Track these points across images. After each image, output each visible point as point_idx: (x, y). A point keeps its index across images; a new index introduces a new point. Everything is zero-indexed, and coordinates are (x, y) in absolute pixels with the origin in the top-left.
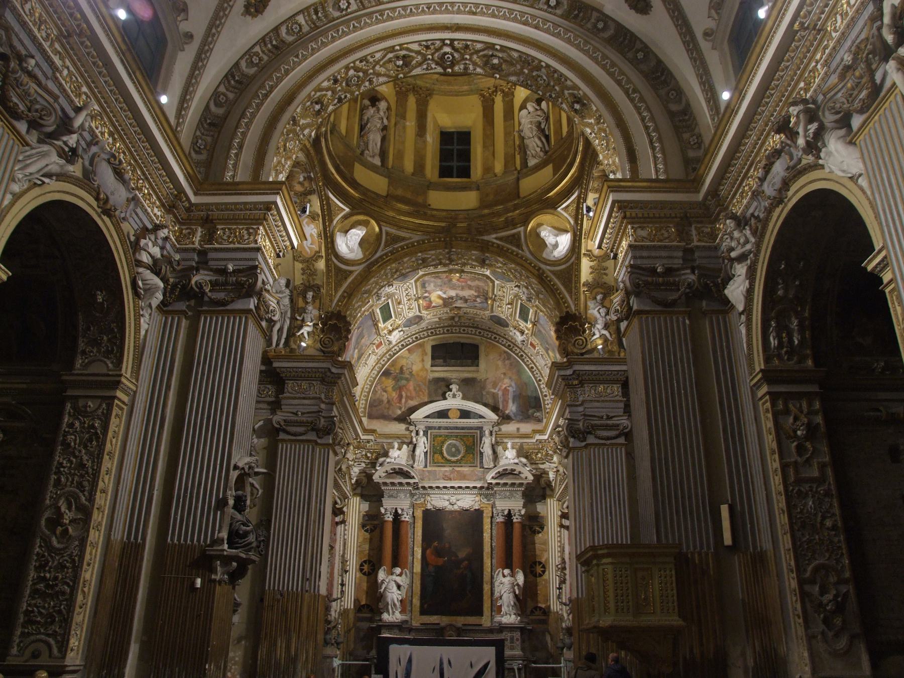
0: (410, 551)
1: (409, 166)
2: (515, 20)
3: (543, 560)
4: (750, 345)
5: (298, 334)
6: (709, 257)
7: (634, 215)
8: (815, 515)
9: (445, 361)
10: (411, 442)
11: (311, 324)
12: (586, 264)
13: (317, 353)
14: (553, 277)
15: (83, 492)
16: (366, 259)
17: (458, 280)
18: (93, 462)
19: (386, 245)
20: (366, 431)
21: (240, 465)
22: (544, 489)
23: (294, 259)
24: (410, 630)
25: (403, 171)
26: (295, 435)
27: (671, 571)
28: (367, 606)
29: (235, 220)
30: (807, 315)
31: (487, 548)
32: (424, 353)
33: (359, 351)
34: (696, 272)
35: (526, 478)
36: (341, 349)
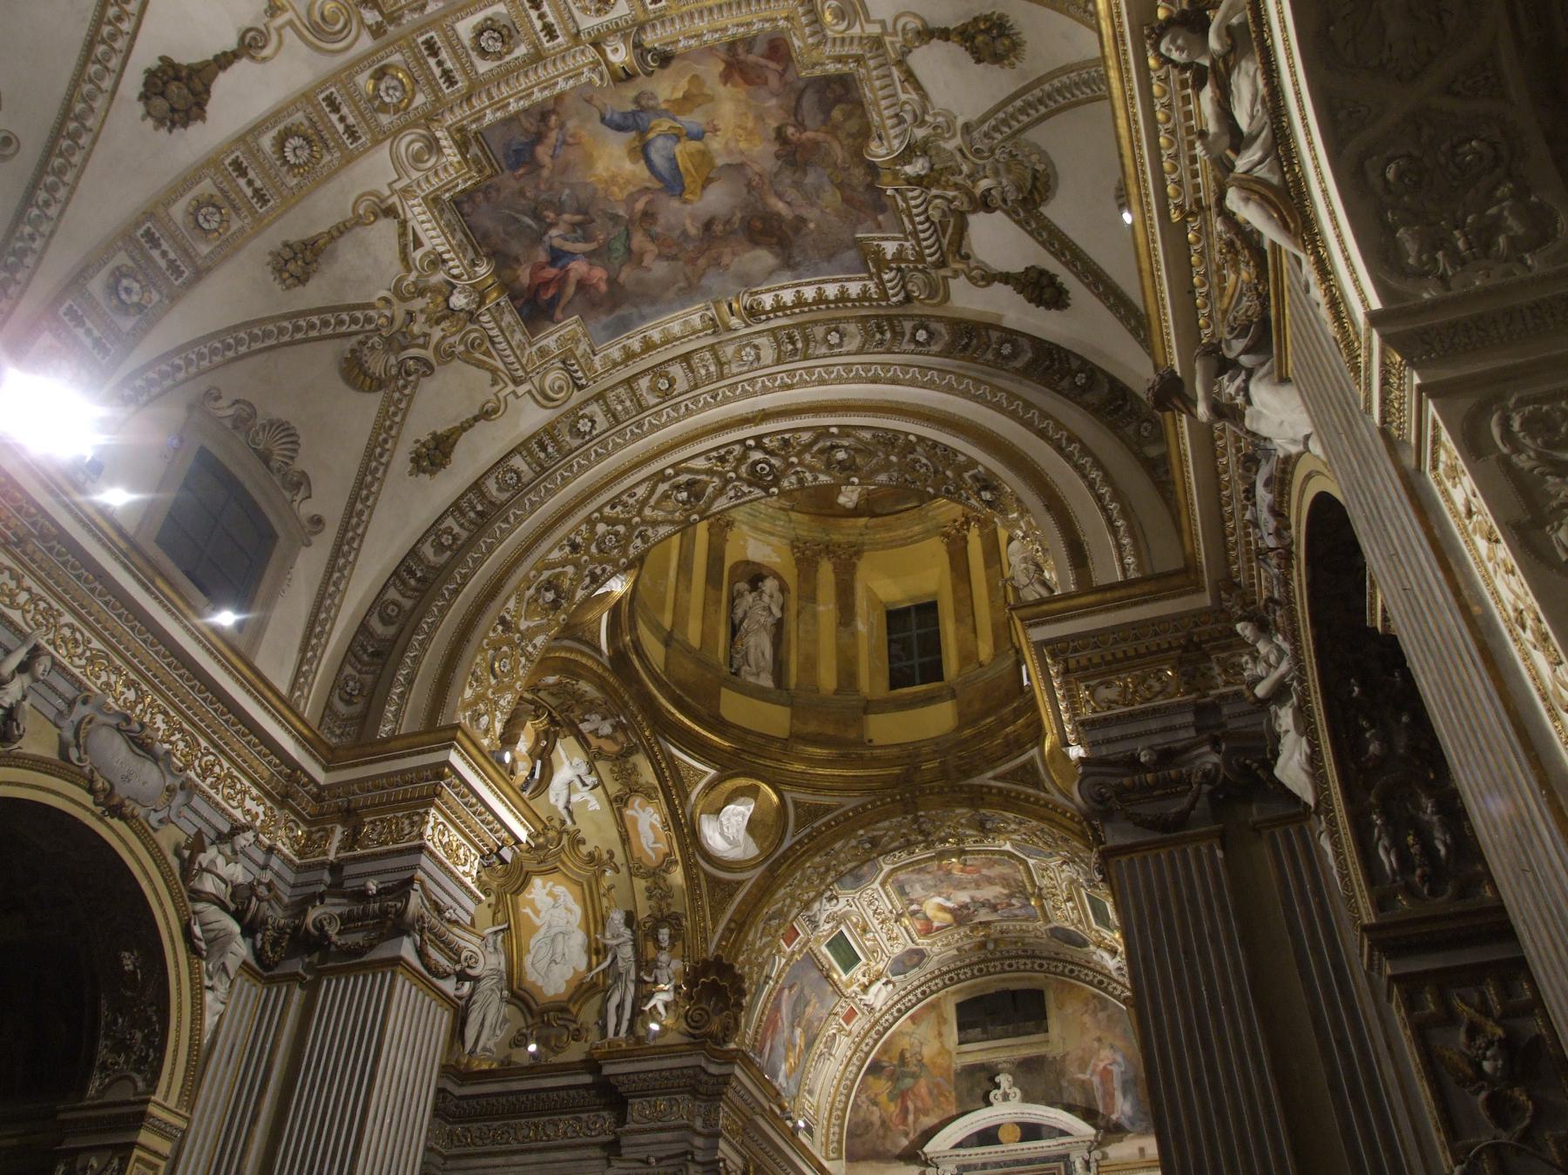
1: (827, 679)
2: (858, 379)
5: (647, 1008)
7: (1083, 662)
9: (985, 1031)
13: (687, 1040)
16: (765, 856)
19: (799, 825)
25: (818, 690)
29: (392, 805)
32: (942, 1020)
33: (805, 1031)
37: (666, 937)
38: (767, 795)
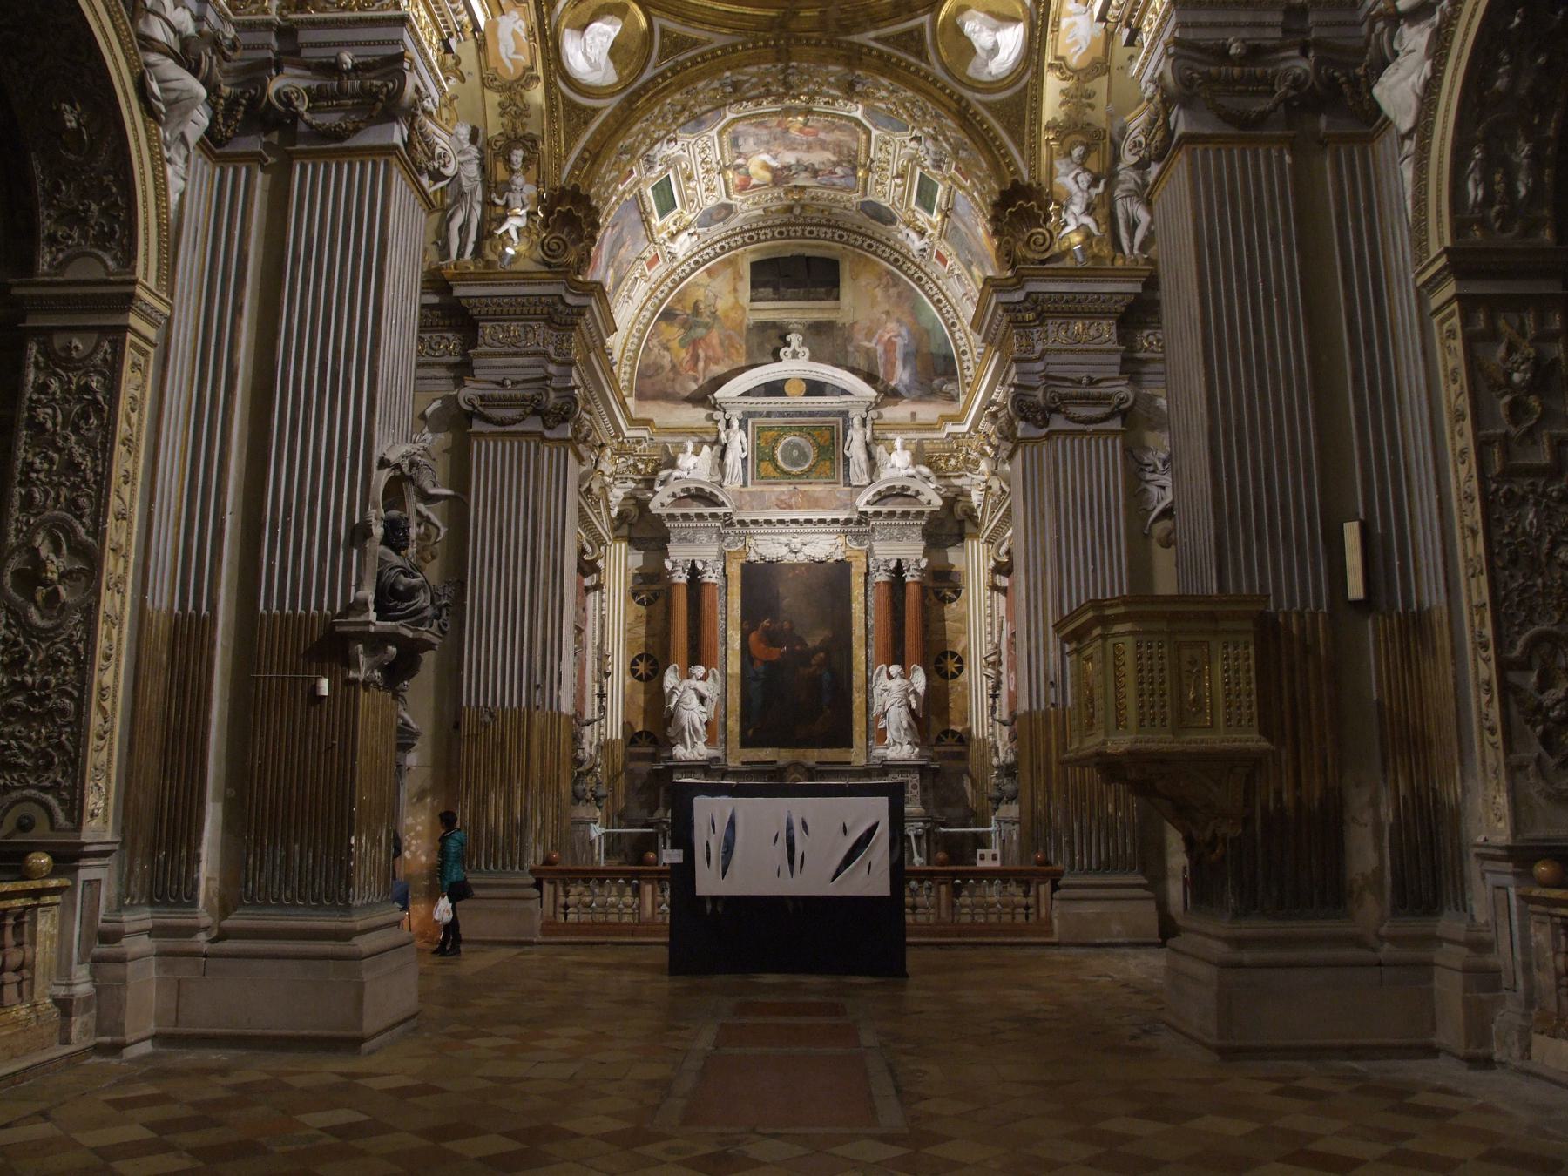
0: (720, 635)
3: (959, 650)
4: (1420, 202)
6: (1340, 24)
8: (1539, 539)
9: (776, 288)
10: (717, 441)
11: (523, 212)
12: (1053, 86)
13: (531, 267)
14: (986, 114)
15: (80, 517)
17: (801, 131)
18: (95, 458)
19: (663, 55)
20: (633, 422)
21: (393, 457)
22: (961, 522)
23: (483, 85)
24: (724, 774)
26: (501, 423)
27: (1247, 648)
28: (646, 734)
30: (1551, 133)
31: (858, 631)
32: (738, 277)
33: (616, 272)
34: (1311, 54)
35: (929, 502)
36: (582, 261)
37: (520, 159)
38: (634, 17)
